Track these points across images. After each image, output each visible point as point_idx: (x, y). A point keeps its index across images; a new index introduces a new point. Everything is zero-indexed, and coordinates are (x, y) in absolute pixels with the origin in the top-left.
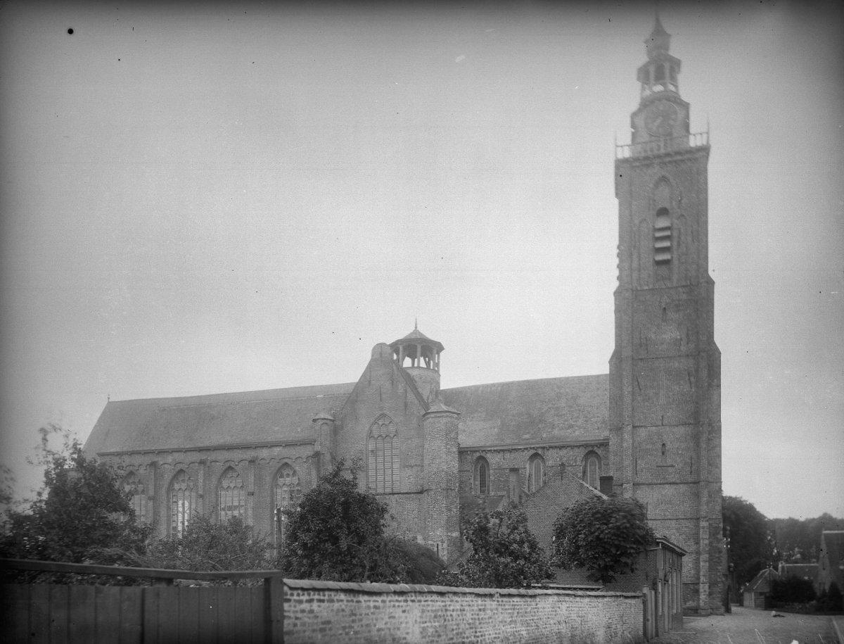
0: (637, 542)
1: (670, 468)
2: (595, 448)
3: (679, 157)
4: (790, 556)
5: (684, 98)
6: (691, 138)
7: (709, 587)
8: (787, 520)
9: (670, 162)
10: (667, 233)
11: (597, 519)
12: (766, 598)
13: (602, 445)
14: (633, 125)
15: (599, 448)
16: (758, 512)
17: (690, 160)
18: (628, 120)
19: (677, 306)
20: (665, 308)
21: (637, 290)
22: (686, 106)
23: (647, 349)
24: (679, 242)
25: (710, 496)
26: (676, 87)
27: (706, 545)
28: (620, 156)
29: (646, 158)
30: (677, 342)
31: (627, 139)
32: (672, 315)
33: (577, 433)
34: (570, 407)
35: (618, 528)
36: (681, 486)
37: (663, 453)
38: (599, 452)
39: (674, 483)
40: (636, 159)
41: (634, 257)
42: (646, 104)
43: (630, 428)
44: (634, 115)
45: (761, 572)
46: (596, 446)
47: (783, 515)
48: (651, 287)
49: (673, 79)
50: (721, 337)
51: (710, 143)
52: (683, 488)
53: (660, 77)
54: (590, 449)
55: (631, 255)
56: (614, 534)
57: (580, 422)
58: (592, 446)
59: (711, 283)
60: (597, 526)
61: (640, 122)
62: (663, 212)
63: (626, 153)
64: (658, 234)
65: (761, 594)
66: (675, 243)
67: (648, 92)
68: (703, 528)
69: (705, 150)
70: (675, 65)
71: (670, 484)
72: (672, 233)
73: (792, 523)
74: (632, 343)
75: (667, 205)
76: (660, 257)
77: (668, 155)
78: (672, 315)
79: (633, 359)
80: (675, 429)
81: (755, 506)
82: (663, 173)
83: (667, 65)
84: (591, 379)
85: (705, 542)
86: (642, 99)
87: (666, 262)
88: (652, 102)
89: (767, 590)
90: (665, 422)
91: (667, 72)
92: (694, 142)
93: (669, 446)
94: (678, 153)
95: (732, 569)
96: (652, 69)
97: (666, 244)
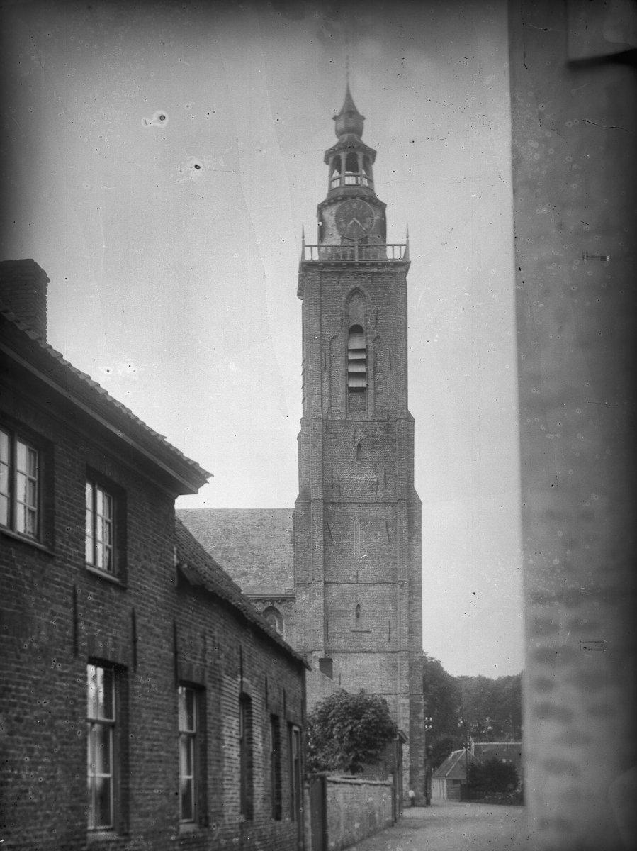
0: (384, 735)
1: (366, 634)
2: (276, 604)
3: (375, 270)
4: (481, 728)
5: (381, 195)
6: (389, 249)
7: (410, 773)
8: (477, 678)
9: (365, 273)
10: (363, 356)
11: (350, 714)
12: (463, 787)
13: (283, 600)
14: (321, 218)
15: (279, 603)
16: (445, 673)
17: (387, 273)
18: (316, 210)
19: (374, 443)
20: (359, 445)
21: (327, 420)
22: (382, 207)
23: (339, 491)
24: (375, 368)
25: (411, 668)
26: (371, 181)
27: (406, 724)
28: (308, 257)
29: (337, 265)
30: (374, 486)
31: (313, 238)
32: (367, 453)
33: (252, 583)
34: (242, 548)
35: (369, 722)
36: (378, 655)
37: (358, 616)
38: (280, 608)
39: (370, 652)
40: (326, 265)
41: (325, 380)
42: (335, 198)
43: (321, 585)
44: (321, 208)
45: (453, 753)
46: (277, 601)
47: (473, 673)
48: (343, 418)
49: (367, 168)
50: (423, 484)
51: (411, 258)
52: (379, 658)
53: (352, 166)
54: (269, 604)
55: (322, 378)
56: (366, 728)
57: (255, 568)
58: (272, 601)
59: (410, 420)
60: (350, 721)
61: (329, 215)
62: (357, 330)
63: (314, 255)
64: (351, 357)
65: (455, 782)
66: (370, 368)
67: (336, 184)
68: (404, 705)
69: (404, 265)
70: (370, 155)
71: (366, 652)
72: (367, 357)
73: (483, 683)
74: (323, 483)
75: (362, 323)
76: (354, 384)
77: (362, 265)
78: (367, 453)
79: (324, 502)
80: (371, 588)
81: (443, 665)
82: (358, 285)
83: (360, 156)
84: (265, 515)
85: (405, 722)
86: (331, 190)
87: (361, 390)
88: (345, 198)
89: (462, 776)
90: (361, 578)
91: (360, 162)
92: (392, 254)
93: (363, 608)
94: (373, 265)
95: (431, 752)
96: (343, 156)
97: (361, 369)
